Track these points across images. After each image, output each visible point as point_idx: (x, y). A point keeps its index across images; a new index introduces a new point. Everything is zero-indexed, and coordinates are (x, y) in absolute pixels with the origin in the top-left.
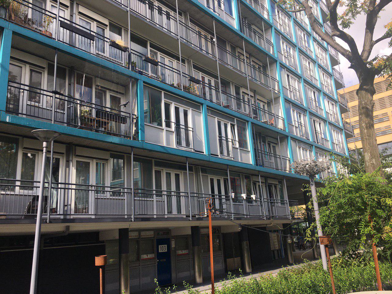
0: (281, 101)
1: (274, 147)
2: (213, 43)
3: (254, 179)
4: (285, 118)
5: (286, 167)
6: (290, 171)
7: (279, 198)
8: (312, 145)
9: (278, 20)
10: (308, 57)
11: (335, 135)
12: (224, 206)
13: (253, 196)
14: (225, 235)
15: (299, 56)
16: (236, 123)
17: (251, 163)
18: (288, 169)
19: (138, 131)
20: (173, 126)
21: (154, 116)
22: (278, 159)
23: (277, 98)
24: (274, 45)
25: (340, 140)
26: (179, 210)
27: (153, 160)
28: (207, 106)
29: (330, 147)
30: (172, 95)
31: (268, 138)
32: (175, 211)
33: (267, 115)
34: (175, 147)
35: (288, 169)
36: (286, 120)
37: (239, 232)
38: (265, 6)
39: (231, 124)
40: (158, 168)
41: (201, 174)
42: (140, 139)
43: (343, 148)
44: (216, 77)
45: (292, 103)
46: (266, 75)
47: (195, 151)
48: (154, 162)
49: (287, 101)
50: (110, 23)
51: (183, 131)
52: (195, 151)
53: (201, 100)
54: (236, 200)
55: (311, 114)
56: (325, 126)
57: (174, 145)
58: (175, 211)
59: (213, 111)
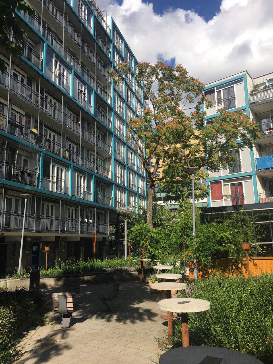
0: (112, 160)
1: (104, 189)
2: (78, 124)
3: (92, 209)
4: (113, 172)
5: (109, 203)
6: (112, 206)
7: (103, 221)
8: (126, 189)
9: (116, 105)
10: (131, 109)
11: (140, 181)
12: (74, 226)
13: (91, 221)
14: (69, 242)
15: (126, 107)
16: (86, 176)
17: (92, 201)
18: (110, 204)
19: (39, 182)
20: (55, 178)
21: (46, 173)
22: (106, 198)
23: (110, 158)
24: (113, 122)
25: (143, 186)
26: (51, 228)
27: (42, 197)
28: (73, 166)
29: (136, 169)
30: (57, 162)
31: (103, 185)
32: (49, 228)
33: (103, 169)
34: (55, 191)
35: (110, 204)
36: (113, 173)
37: (77, 241)
38: (110, 95)
39: (84, 177)
40: (44, 202)
41: (65, 206)
42: (40, 187)
43: (144, 191)
44: (77, 144)
45: (118, 161)
46: (105, 143)
47: (65, 193)
48: (44, 201)
49: (116, 160)
50: (26, 113)
51: (59, 181)
52: (65, 193)
53: (71, 163)
54: (82, 222)
55: (128, 168)
56: (135, 156)
57: (55, 190)
58: (49, 228)
59: (76, 169)
